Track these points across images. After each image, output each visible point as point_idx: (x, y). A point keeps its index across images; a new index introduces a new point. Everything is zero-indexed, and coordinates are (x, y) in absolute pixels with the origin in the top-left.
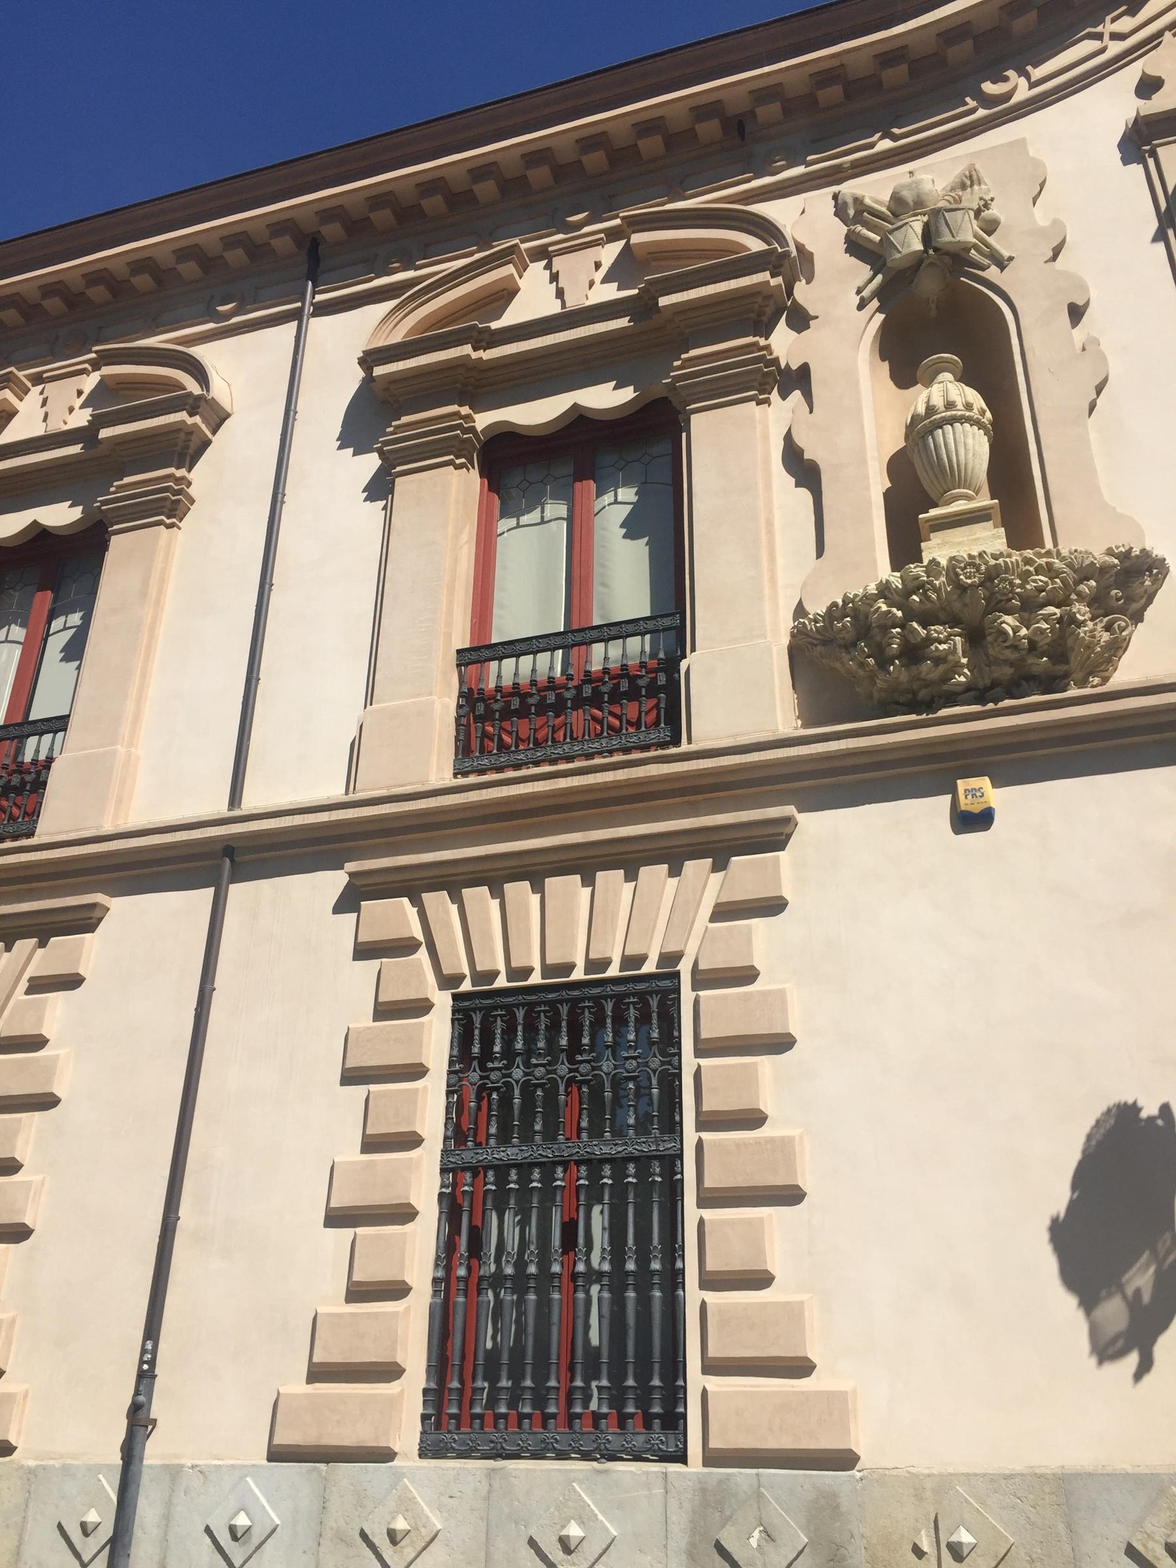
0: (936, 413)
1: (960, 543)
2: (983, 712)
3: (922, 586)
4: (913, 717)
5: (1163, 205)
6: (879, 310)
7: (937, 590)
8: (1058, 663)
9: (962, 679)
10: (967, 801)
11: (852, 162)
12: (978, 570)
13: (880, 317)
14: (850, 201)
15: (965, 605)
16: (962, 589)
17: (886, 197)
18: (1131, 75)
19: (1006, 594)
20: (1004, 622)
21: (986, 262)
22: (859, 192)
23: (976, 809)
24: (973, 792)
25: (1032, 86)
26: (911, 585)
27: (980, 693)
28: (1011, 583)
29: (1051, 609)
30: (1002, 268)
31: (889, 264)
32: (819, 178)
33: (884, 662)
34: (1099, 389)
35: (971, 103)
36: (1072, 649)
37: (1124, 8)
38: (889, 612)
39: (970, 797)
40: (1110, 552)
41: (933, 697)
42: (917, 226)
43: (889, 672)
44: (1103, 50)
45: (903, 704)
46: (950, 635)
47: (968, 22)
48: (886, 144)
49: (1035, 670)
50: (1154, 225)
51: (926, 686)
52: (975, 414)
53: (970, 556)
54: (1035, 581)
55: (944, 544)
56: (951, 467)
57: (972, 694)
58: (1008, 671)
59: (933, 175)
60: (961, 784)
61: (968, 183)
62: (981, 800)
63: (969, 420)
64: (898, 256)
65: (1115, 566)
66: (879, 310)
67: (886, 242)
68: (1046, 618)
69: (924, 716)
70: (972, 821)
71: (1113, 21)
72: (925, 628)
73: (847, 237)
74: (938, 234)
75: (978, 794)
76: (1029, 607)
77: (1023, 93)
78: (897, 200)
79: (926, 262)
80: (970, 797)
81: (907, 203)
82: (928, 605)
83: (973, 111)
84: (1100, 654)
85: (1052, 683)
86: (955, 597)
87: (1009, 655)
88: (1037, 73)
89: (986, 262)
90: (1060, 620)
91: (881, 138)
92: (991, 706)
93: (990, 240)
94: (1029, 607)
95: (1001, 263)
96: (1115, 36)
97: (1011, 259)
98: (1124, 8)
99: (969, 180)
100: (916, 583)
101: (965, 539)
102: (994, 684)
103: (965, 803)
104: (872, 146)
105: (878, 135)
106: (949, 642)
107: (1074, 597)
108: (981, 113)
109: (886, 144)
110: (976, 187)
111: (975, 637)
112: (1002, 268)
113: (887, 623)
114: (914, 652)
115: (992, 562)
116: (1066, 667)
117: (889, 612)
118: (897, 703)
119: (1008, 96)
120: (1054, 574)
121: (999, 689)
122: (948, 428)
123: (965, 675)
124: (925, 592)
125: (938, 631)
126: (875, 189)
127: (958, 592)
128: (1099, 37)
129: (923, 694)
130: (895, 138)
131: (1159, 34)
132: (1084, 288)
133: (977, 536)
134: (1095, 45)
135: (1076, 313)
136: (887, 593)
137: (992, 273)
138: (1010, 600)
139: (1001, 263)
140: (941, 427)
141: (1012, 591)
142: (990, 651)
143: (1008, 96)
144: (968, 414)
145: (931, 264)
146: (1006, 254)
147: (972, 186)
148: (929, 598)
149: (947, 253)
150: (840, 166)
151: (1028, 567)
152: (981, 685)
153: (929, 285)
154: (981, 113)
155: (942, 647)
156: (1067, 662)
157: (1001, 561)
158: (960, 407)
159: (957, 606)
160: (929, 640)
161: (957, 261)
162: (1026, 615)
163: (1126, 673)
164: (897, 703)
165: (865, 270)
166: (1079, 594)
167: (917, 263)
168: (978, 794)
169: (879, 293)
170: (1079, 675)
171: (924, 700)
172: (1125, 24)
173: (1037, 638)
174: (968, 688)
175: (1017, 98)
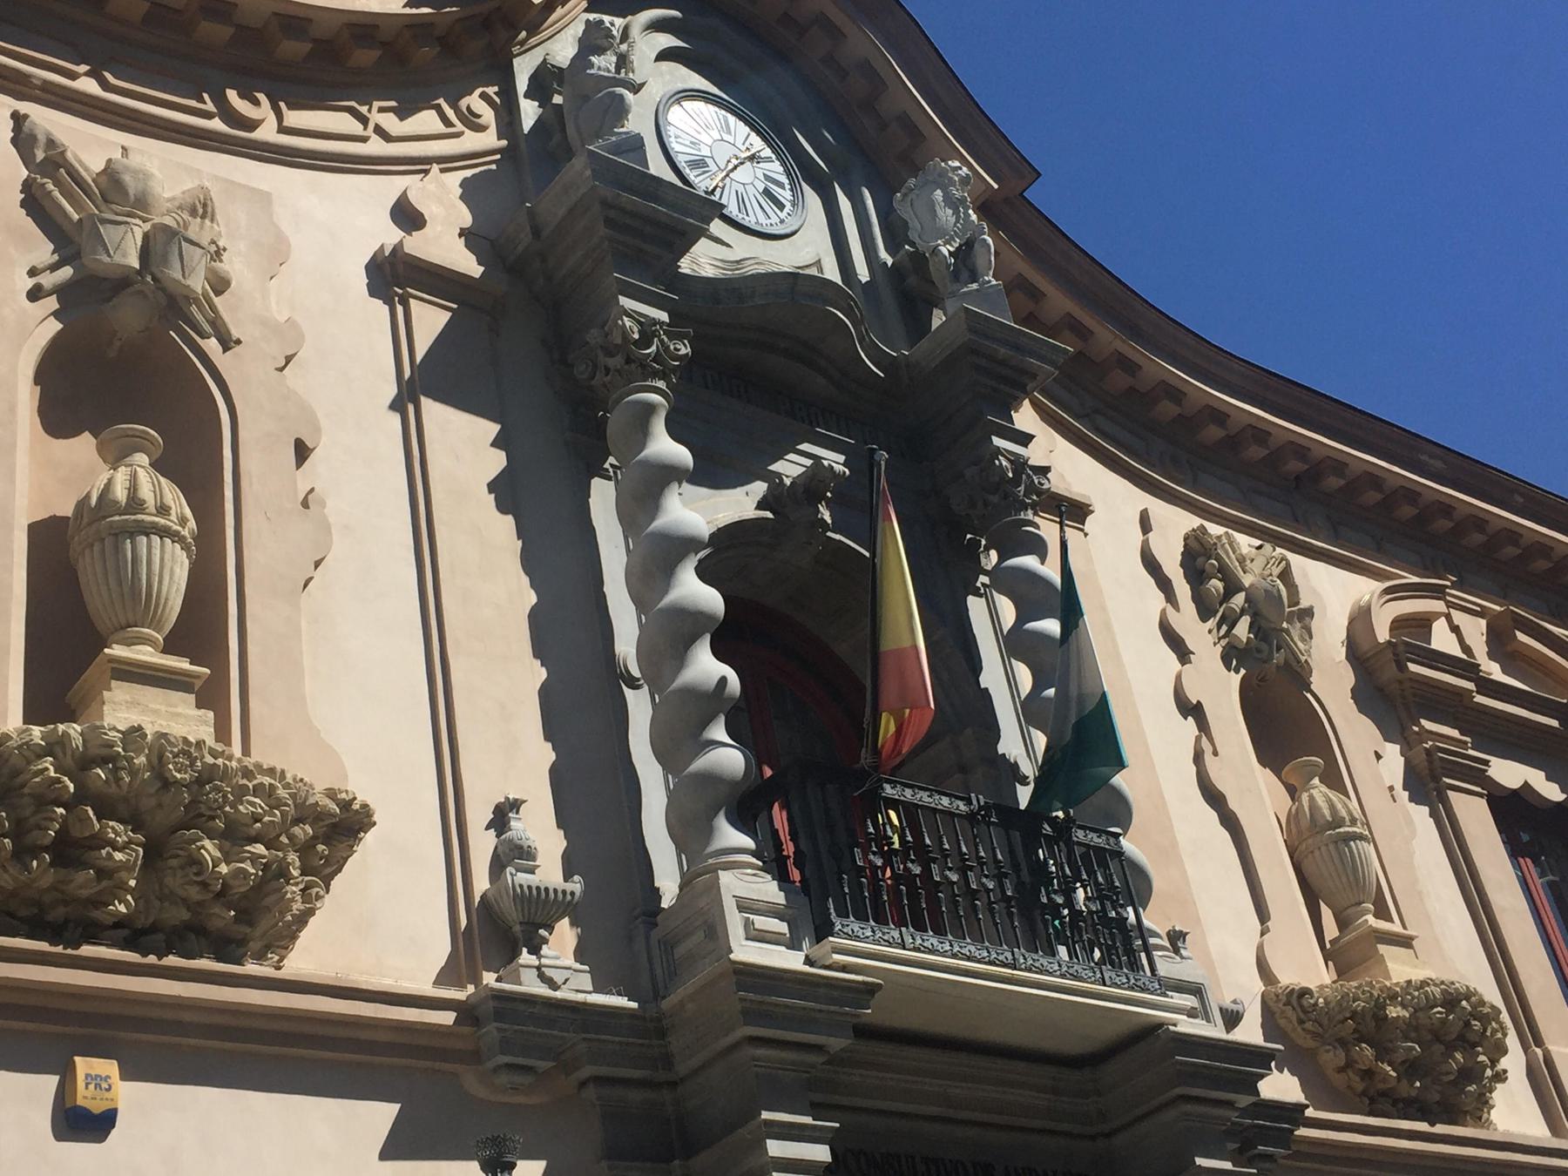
0: (143, 511)
1: (156, 712)
2: (139, 965)
3: (114, 758)
4: (43, 946)
5: (407, 373)
6: (56, 314)
7: (133, 772)
8: (249, 920)
9: (122, 908)
10: (88, 1094)
11: (45, 82)
12: (192, 765)
13: (55, 326)
14: (42, 138)
15: (160, 805)
16: (166, 783)
17: (97, 165)
18: (390, 187)
19: (211, 809)
20: (203, 847)
21: (207, 328)
22: (61, 137)
23: (97, 1107)
24: (96, 1080)
25: (283, 130)
26: (95, 751)
27: (132, 934)
28: (225, 797)
29: (259, 849)
30: (226, 349)
31: (85, 261)
32: (53, 94)
33: (23, 853)
34: (317, 564)
35: (210, 106)
36: (269, 909)
37: (393, 103)
38: (58, 781)
39: (92, 1087)
40: (331, 794)
41: (67, 921)
42: (139, 231)
43: (28, 868)
44: (364, 140)
45: (21, 919)
46: (130, 842)
47: (310, 20)
48: (89, 86)
49: (216, 924)
50: (392, 391)
51: (66, 903)
52: (185, 533)
53: (185, 740)
54: (253, 804)
55: (133, 704)
56: (149, 594)
57: (125, 932)
58: (185, 915)
59: (168, 171)
60: (83, 1065)
61: (201, 211)
62: (107, 1095)
63: (164, 532)
64: (106, 259)
65: (334, 815)
66: (56, 314)
67: (90, 226)
68: (254, 859)
69: (59, 949)
70: (82, 1123)
71: (381, 110)
72: (99, 820)
73: (26, 181)
74: (165, 261)
75: (104, 1085)
76: (235, 836)
77: (267, 132)
78: (111, 178)
79: (137, 287)
80: (92, 1087)
81: (127, 194)
82: (113, 789)
83: (208, 115)
84: (289, 925)
85: (228, 948)
86: (152, 791)
87: (194, 893)
88: (294, 118)
89: (207, 328)
90: (266, 867)
91: (87, 74)
92: (152, 959)
93: (216, 300)
94: (235, 836)
95: (227, 343)
96: (379, 130)
97: (238, 342)
98: (393, 103)
99: (201, 208)
100: (104, 751)
101: (163, 708)
102: (154, 929)
103: (85, 1096)
104: (74, 76)
105: (84, 68)
106: (123, 848)
107: (284, 839)
108: (217, 124)
109: (89, 86)
110: (207, 222)
111: (155, 852)
112: (226, 349)
113: (47, 797)
114: (71, 850)
115: (209, 760)
116: (248, 930)
117: (58, 781)
118: (11, 915)
119: (252, 125)
120: (273, 802)
121: (161, 936)
122: (156, 539)
123: (127, 905)
124: (116, 769)
125: (117, 830)
126: (91, 146)
127: (159, 785)
128: (364, 121)
129: (58, 914)
130: (105, 85)
131: (428, 160)
132: (317, 430)
133: (180, 710)
134: (355, 127)
135: (302, 452)
136: (58, 750)
137: (211, 345)
138: (213, 818)
139: (227, 343)
140: (147, 535)
141: (221, 808)
142: (169, 880)
143: (252, 125)
144: (162, 521)
145: (141, 292)
146: (235, 334)
147: (203, 217)
148: (118, 780)
149: (163, 290)
150: (27, 76)
151: (245, 781)
152: (140, 923)
153: (128, 317)
154: (217, 124)
155: (118, 856)
156: (251, 924)
157: (220, 761)
158: (173, 517)
159: (148, 803)
160: (99, 841)
161: (175, 307)
162: (227, 844)
163: (302, 961)
164: (11, 915)
165: (44, 251)
166: (291, 838)
167: (122, 283)
168: (104, 1085)
169: (61, 291)
170: (255, 945)
171: (68, 925)
172: (390, 122)
173: (231, 882)
174: (120, 923)
175: (259, 134)
